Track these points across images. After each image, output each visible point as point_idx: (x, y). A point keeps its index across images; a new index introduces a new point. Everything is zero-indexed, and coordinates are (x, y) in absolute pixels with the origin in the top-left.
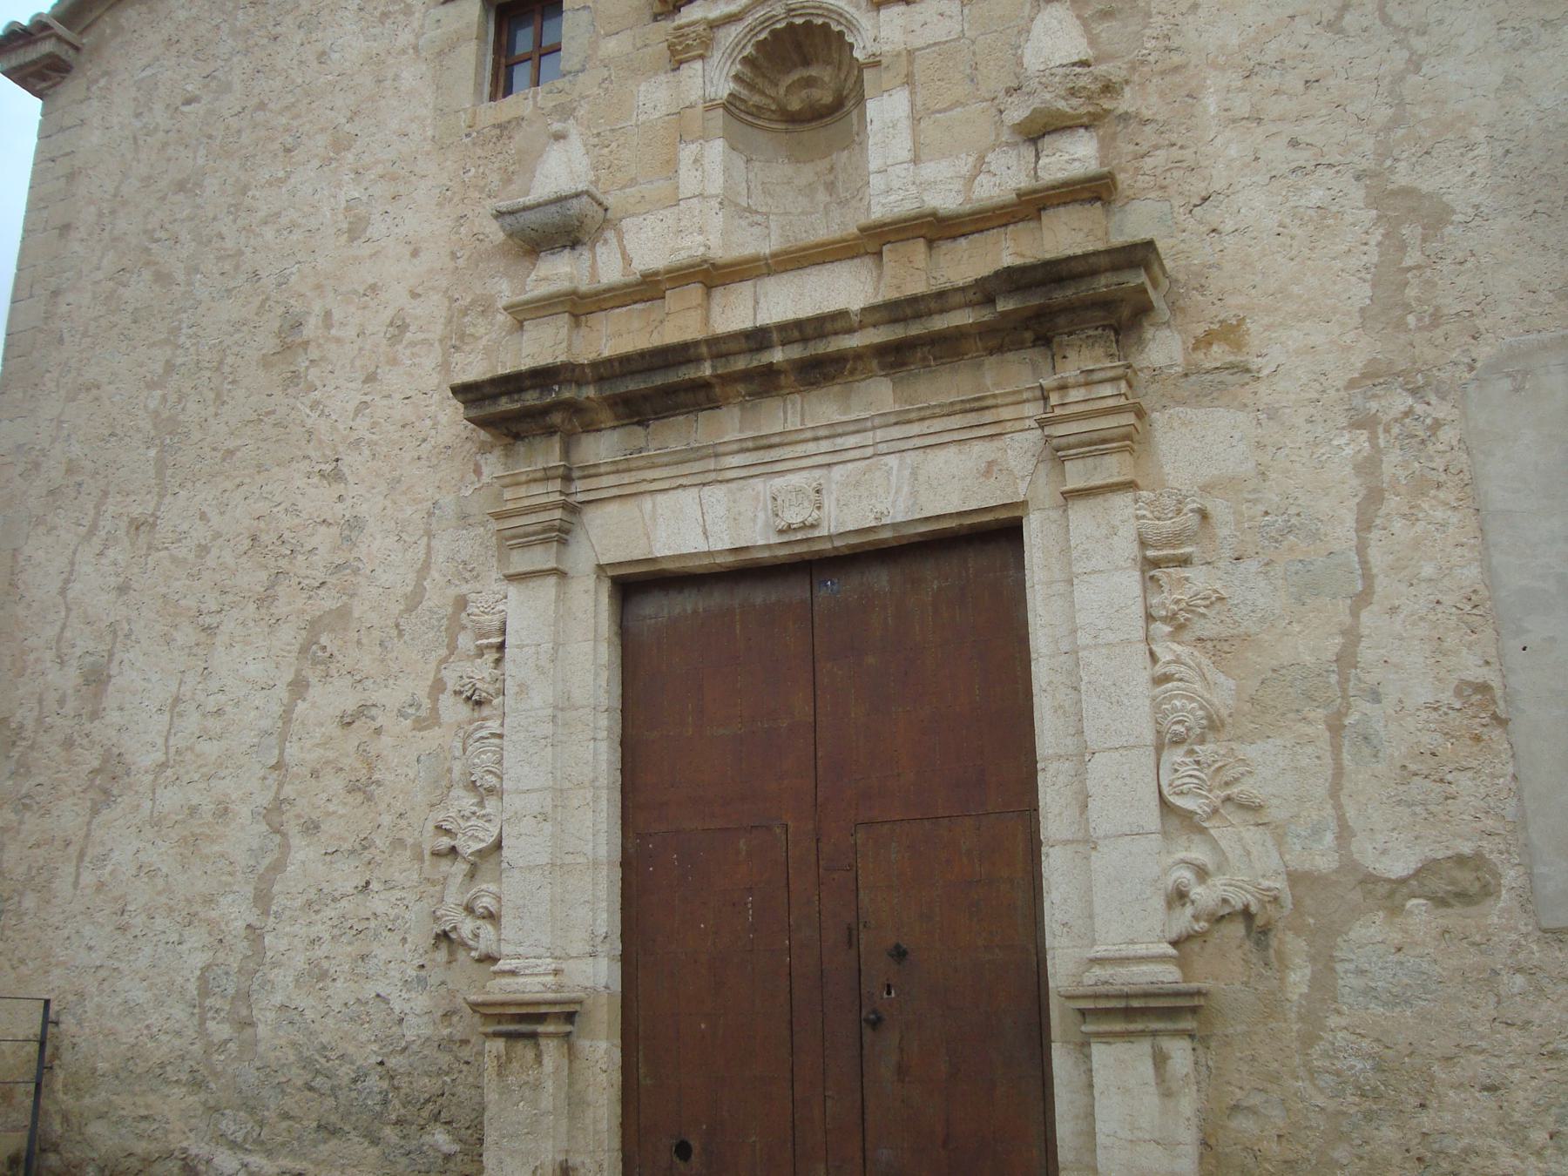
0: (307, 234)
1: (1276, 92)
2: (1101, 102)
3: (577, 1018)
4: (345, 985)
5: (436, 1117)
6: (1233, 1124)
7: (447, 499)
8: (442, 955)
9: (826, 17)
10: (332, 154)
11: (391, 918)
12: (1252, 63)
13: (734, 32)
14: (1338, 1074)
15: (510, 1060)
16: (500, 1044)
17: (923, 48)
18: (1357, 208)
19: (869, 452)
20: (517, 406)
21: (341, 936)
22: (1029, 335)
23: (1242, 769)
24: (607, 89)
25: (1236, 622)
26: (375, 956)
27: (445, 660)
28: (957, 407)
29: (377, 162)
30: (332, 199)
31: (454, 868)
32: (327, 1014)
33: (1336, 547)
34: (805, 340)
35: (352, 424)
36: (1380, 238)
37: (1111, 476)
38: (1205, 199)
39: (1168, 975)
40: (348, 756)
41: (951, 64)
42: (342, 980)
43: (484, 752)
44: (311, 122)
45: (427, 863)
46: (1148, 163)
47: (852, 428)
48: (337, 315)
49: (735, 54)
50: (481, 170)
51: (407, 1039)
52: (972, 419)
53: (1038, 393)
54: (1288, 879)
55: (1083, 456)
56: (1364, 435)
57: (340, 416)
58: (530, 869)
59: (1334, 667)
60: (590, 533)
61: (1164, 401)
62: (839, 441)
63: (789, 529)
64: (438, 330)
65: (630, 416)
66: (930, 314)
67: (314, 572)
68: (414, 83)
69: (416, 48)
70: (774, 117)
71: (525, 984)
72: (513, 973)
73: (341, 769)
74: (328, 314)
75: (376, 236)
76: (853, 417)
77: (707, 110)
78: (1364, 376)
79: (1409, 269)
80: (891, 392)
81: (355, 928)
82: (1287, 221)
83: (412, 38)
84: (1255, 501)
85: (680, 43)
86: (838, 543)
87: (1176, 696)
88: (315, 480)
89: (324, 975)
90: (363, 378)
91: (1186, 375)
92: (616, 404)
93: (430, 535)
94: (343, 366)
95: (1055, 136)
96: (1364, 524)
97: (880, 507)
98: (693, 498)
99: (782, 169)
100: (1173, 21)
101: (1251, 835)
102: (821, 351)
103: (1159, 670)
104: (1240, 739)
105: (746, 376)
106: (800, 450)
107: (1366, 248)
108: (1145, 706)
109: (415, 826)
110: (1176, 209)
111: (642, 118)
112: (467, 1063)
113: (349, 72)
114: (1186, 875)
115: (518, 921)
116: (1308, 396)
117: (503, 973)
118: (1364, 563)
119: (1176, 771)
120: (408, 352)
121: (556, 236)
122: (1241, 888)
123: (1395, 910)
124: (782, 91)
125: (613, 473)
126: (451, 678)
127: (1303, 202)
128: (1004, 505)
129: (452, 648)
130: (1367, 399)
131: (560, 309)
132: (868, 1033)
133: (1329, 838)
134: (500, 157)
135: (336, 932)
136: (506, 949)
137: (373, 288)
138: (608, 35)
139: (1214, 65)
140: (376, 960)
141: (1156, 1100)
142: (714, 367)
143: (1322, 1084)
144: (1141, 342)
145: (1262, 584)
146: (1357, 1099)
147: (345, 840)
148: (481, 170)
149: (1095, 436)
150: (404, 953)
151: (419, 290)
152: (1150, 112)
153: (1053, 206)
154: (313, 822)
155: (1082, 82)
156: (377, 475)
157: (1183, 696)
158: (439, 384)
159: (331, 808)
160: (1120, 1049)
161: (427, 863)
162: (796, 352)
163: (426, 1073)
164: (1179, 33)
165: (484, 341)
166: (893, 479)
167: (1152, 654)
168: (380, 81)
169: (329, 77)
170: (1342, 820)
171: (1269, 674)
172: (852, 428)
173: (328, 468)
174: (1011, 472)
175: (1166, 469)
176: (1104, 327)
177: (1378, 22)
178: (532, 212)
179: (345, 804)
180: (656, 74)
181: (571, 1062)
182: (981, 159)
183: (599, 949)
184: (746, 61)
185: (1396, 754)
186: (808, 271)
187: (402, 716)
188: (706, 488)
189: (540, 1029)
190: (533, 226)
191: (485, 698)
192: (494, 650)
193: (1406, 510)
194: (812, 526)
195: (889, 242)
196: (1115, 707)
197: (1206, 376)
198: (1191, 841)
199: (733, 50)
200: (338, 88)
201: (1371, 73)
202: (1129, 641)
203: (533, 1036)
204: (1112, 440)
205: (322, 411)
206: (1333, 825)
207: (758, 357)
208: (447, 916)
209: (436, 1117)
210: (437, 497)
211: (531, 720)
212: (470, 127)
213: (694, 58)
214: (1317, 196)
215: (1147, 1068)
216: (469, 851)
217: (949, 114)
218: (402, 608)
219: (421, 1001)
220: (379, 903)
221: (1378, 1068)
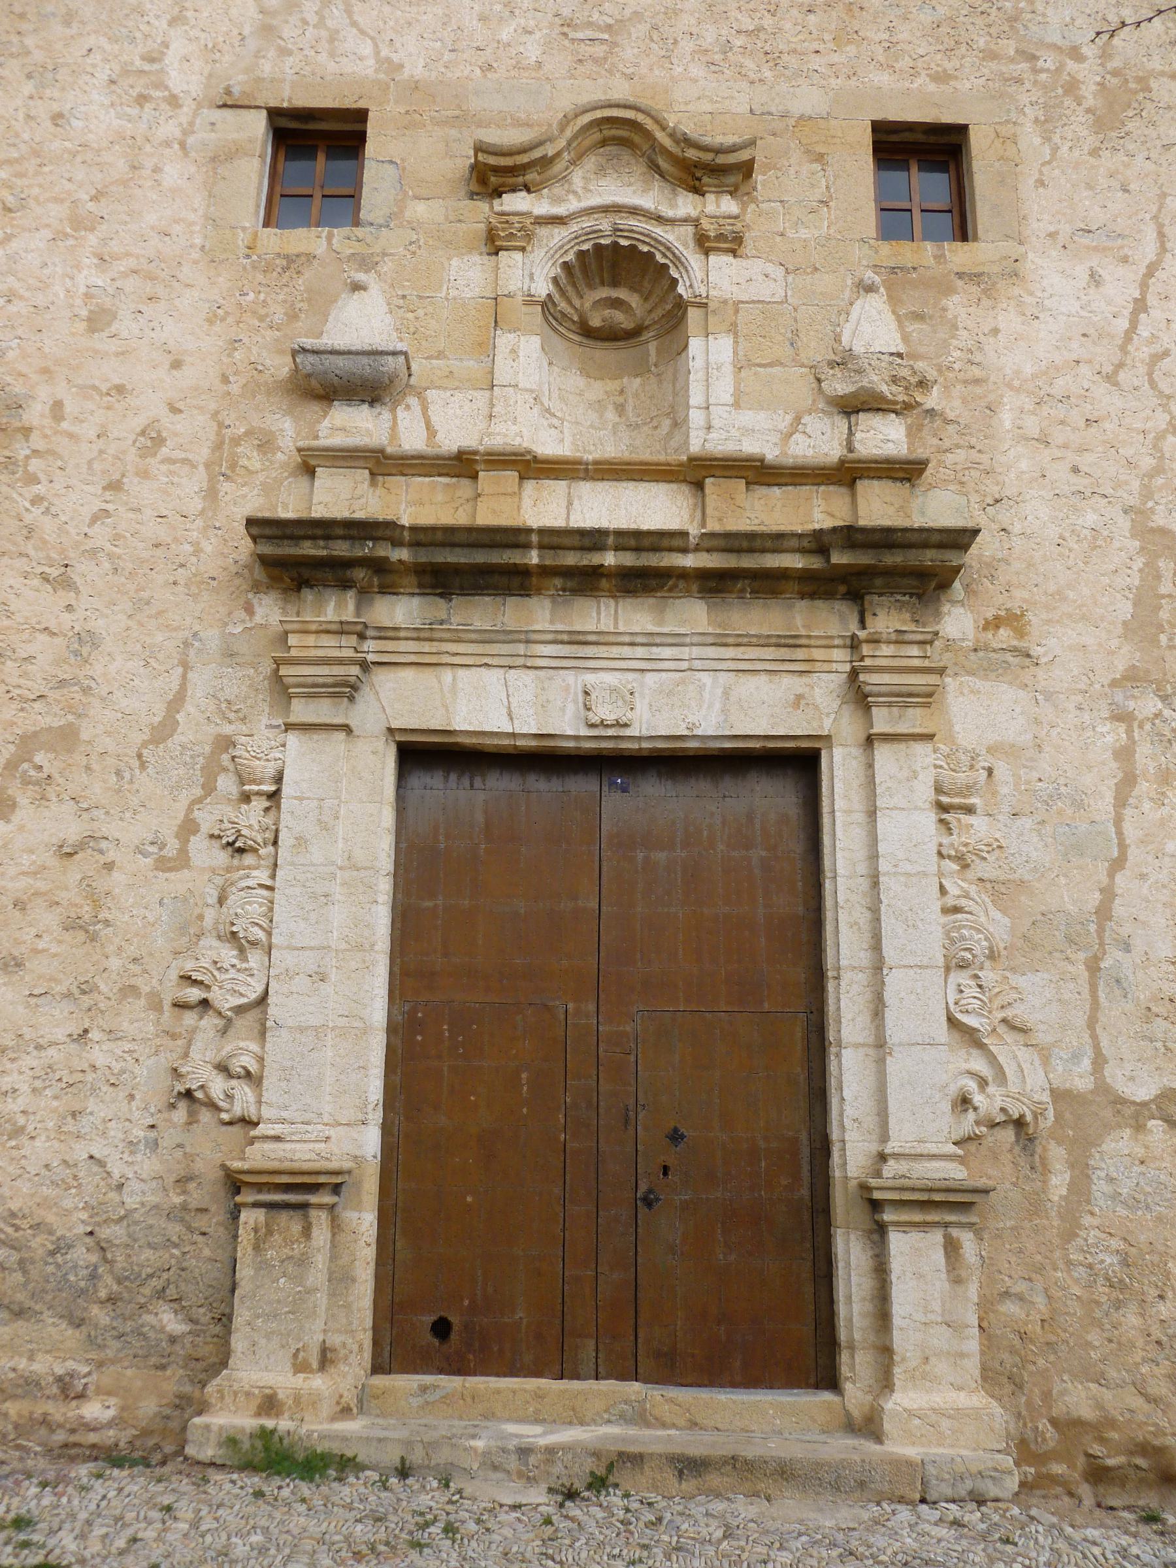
0: (32, 309)
1: (1062, 422)
2: (916, 394)
3: (344, 1188)
4: (47, 1144)
5: (160, 1294)
6: (1002, 1308)
7: (212, 636)
8: (180, 1114)
9: (652, 246)
10: (68, 230)
11: (116, 1071)
12: (1042, 393)
13: (558, 235)
14: (1090, 1266)
15: (270, 1232)
16: (260, 1215)
17: (747, 302)
18: (1124, 537)
19: (685, 665)
20: (325, 553)
21: (45, 1088)
22: (842, 589)
23: (1016, 996)
24: (414, 253)
25: (1011, 869)
26: (91, 1113)
27: (200, 800)
28: (773, 640)
29: (128, 254)
30: (67, 280)
31: (203, 1023)
32: (20, 1176)
33: (1097, 818)
34: (637, 549)
35: (86, 530)
36: (1141, 565)
37: (914, 726)
38: (997, 501)
39: (956, 1173)
40: (67, 889)
41: (773, 325)
42: (43, 1138)
43: (250, 903)
44: (40, 186)
45: (167, 1014)
46: (950, 458)
47: (670, 640)
48: (69, 408)
49: (557, 256)
50: (262, 296)
51: (127, 1207)
52: (784, 653)
53: (848, 642)
54: (1052, 1095)
55: (890, 705)
56: (1122, 728)
57: (72, 519)
58: (302, 1030)
59: (1094, 918)
60: (381, 695)
61: (956, 669)
62: (655, 649)
63: (603, 724)
64: (203, 453)
65: (433, 587)
66: (763, 551)
67: (30, 683)
68: (179, 181)
69: (183, 145)
70: (573, 328)
71: (294, 1151)
72: (277, 1139)
73: (57, 903)
74: (58, 406)
75: (125, 334)
76: (666, 630)
77: (527, 303)
78: (1125, 678)
79: (1163, 596)
80: (705, 614)
81: (65, 1080)
82: (1067, 535)
83: (178, 133)
84: (1032, 768)
85: (503, 230)
86: (645, 745)
87: (964, 927)
88: (36, 582)
89: (19, 1131)
90: (104, 483)
91: (975, 650)
92: (424, 572)
93: (186, 666)
94: (77, 466)
95: (869, 415)
96: (1121, 802)
97: (691, 719)
98: (498, 679)
99: (575, 380)
100: (976, 338)
101: (1023, 1054)
102: (654, 564)
103: (950, 902)
104: (1013, 970)
105: (567, 573)
106: (615, 651)
107: (1129, 571)
108: (939, 933)
109: (154, 973)
110: (972, 504)
111: (453, 293)
112: (204, 1234)
113: (95, 145)
114: (972, 1085)
115: (284, 1084)
116: (1079, 686)
117: (266, 1138)
118: (1120, 834)
119: (961, 991)
120: (164, 468)
121: (359, 388)
122: (1018, 1100)
123: (1139, 1128)
124: (588, 305)
125: (413, 639)
126: (207, 819)
127: (1080, 522)
128: (808, 736)
129: (209, 788)
130: (1126, 698)
131: (361, 463)
132: (643, 1210)
133: (1086, 1064)
134: (285, 289)
135: (38, 1084)
136: (266, 1112)
137: (120, 389)
138: (417, 198)
139: (1010, 386)
140: (91, 1118)
141: (947, 1285)
142: (539, 556)
143: (1076, 1275)
144: (938, 615)
145: (1035, 839)
146: (1107, 1290)
147: (58, 981)
148: (262, 296)
149: (904, 689)
150: (130, 1110)
151: (180, 405)
152: (953, 414)
153: (869, 477)
154: (14, 959)
155: (905, 372)
156: (119, 591)
157: (971, 928)
158: (203, 509)
159: (41, 945)
160: (915, 1237)
161: (167, 1014)
162: (628, 559)
163: (149, 1245)
164: (980, 349)
165: (261, 477)
166: (706, 695)
167: (942, 887)
168: (135, 167)
169: (68, 144)
170: (1097, 1047)
171: (1039, 917)
172: (670, 640)
173: (54, 572)
174: (816, 707)
175: (957, 728)
176: (911, 595)
177: (1146, 384)
178: (341, 357)
179: (60, 942)
180: (470, 252)
181: (334, 1235)
182: (798, 419)
183: (370, 1117)
184: (566, 266)
185: (1142, 997)
186: (624, 484)
187: (140, 853)
188: (512, 671)
189: (313, 1199)
190: (337, 372)
191: (251, 847)
192: (264, 798)
193: (1153, 794)
194: (626, 725)
195: (713, 476)
196: (910, 930)
197: (992, 654)
198: (969, 1054)
199: (556, 252)
200: (79, 159)
201: (1139, 425)
202: (925, 874)
203: (304, 1206)
204: (918, 696)
205: (47, 509)
206: (1090, 1052)
207: (589, 556)
208: (194, 1073)
209: (160, 1294)
210: (196, 628)
211: (309, 875)
212: (249, 248)
213: (515, 248)
214: (1091, 519)
215: (938, 1257)
216: (227, 1006)
217: (769, 370)
218: (146, 738)
219: (148, 1165)
220: (100, 1055)
221: (1125, 1263)
